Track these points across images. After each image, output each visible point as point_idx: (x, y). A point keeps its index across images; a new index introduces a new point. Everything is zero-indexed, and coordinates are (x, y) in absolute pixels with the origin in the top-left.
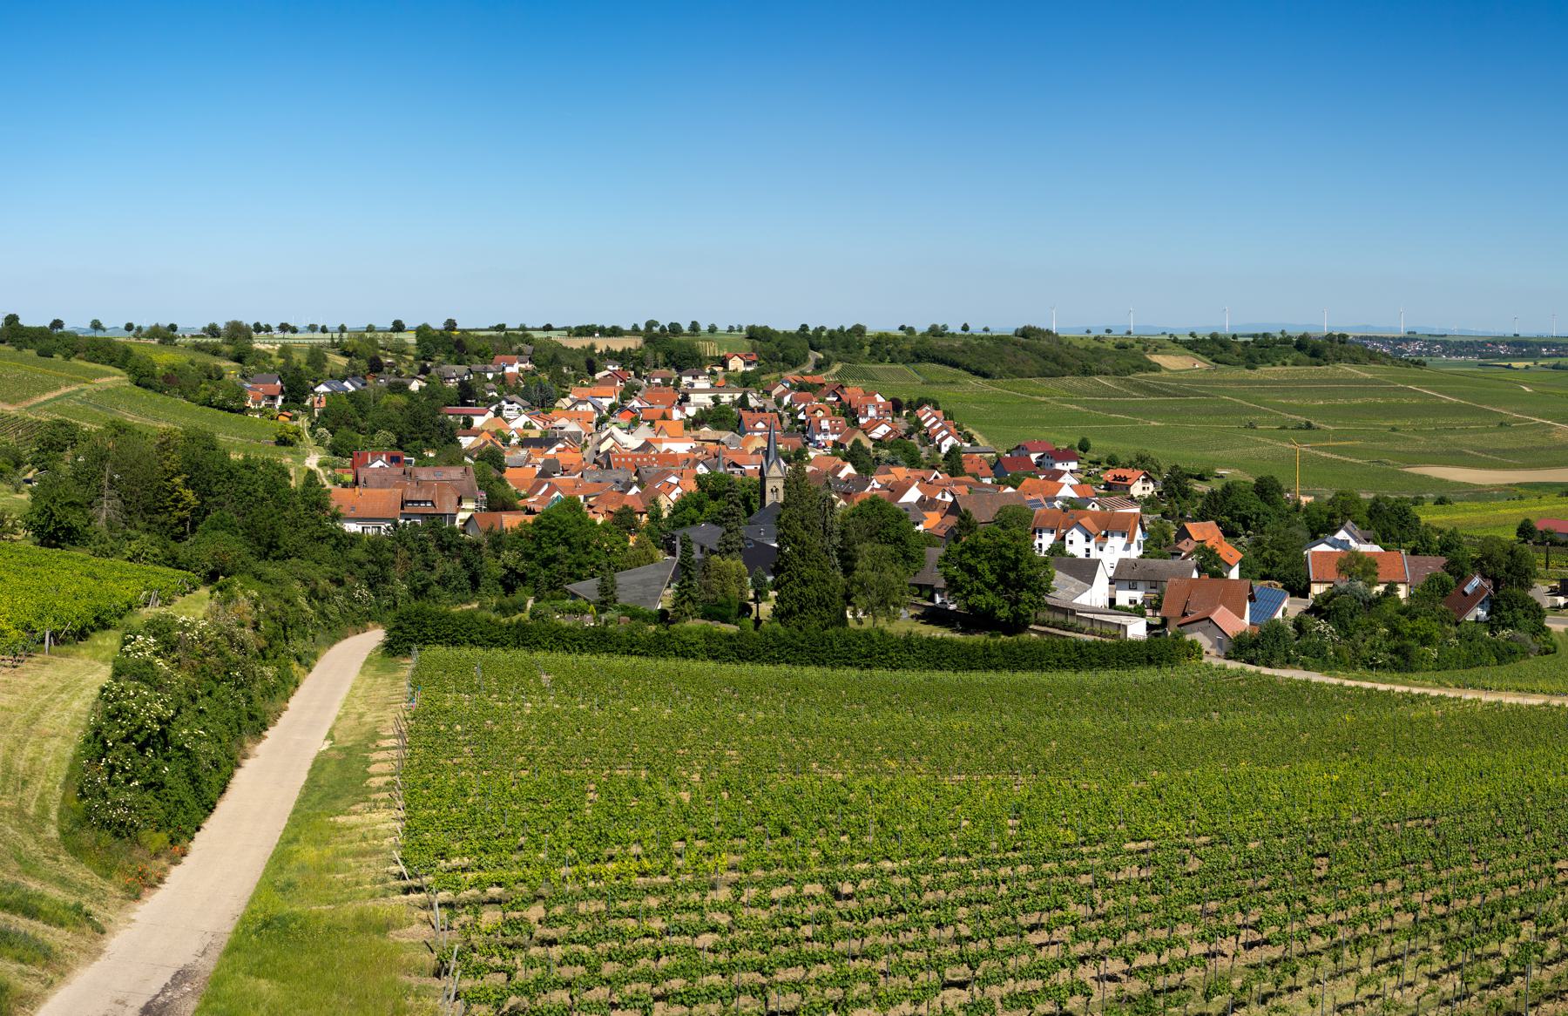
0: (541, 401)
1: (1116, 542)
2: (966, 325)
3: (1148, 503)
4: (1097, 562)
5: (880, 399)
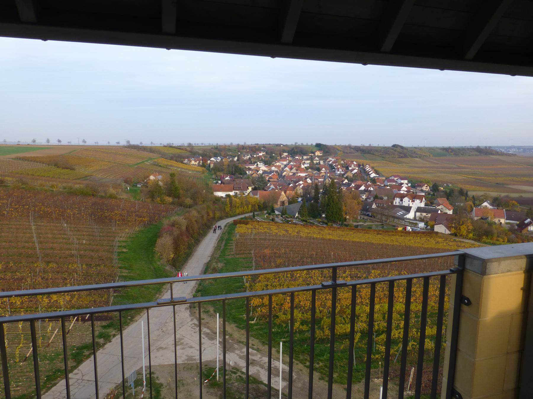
0: (267, 163)
1: (417, 201)
2: (58, 140)
3: (427, 193)
4: (411, 207)
5: (355, 163)
